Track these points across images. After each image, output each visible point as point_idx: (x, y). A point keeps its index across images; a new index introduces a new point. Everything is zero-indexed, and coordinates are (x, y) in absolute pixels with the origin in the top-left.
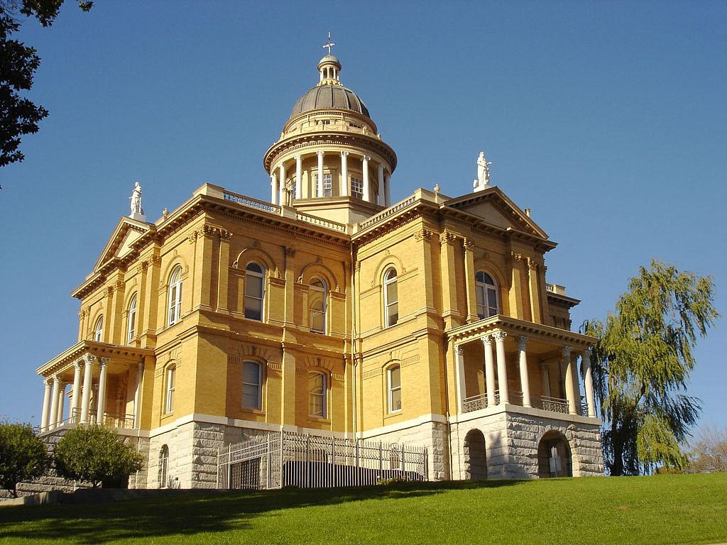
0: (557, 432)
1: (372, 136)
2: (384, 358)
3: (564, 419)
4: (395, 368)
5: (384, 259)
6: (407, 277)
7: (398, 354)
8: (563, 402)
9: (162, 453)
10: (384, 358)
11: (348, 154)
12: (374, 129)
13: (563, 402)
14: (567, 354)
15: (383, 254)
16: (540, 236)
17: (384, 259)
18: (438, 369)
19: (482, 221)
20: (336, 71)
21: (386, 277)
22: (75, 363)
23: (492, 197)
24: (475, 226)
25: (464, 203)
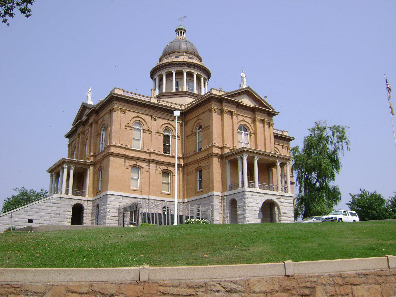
0: (271, 200)
1: (199, 63)
2: (196, 166)
3: (53, 165)
4: (201, 171)
5: (196, 122)
6: (206, 129)
7: (201, 165)
8: (252, 183)
9: (97, 207)
10: (196, 166)
11: (197, 74)
12: (201, 60)
13: (252, 183)
14: (278, 164)
15: (196, 119)
16: (270, 110)
17: (196, 122)
18: (163, 165)
19: (242, 103)
20: (184, 33)
21: (198, 129)
22: (60, 168)
23: (247, 91)
24: (238, 105)
25: (233, 95)
